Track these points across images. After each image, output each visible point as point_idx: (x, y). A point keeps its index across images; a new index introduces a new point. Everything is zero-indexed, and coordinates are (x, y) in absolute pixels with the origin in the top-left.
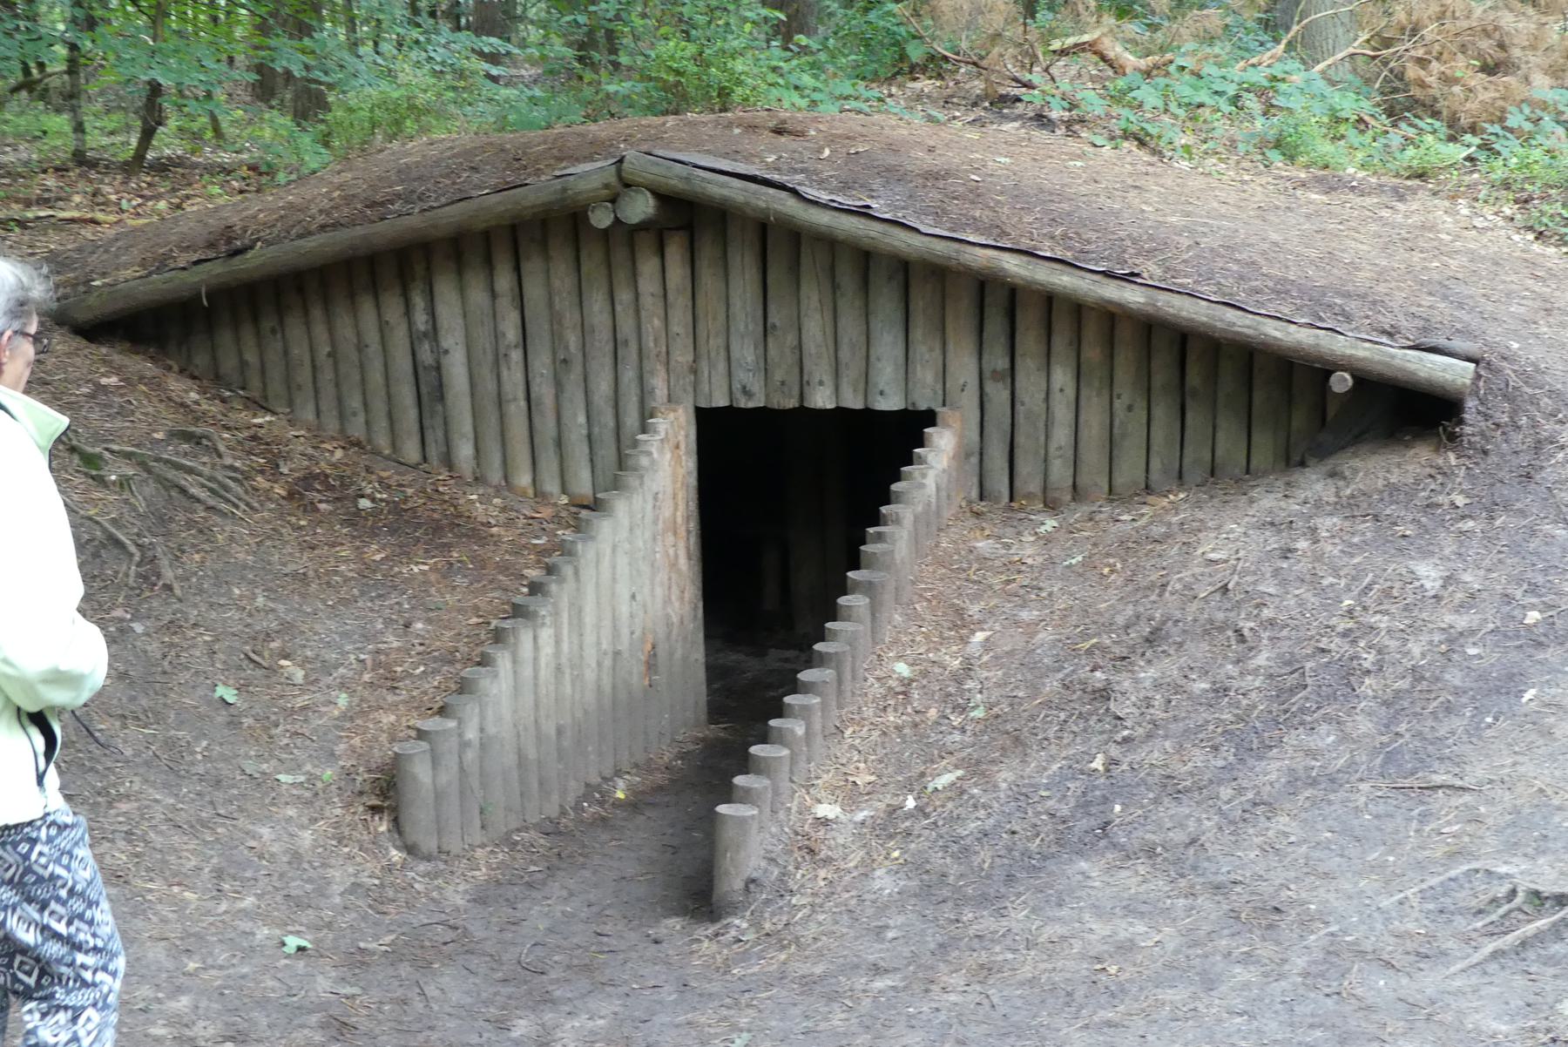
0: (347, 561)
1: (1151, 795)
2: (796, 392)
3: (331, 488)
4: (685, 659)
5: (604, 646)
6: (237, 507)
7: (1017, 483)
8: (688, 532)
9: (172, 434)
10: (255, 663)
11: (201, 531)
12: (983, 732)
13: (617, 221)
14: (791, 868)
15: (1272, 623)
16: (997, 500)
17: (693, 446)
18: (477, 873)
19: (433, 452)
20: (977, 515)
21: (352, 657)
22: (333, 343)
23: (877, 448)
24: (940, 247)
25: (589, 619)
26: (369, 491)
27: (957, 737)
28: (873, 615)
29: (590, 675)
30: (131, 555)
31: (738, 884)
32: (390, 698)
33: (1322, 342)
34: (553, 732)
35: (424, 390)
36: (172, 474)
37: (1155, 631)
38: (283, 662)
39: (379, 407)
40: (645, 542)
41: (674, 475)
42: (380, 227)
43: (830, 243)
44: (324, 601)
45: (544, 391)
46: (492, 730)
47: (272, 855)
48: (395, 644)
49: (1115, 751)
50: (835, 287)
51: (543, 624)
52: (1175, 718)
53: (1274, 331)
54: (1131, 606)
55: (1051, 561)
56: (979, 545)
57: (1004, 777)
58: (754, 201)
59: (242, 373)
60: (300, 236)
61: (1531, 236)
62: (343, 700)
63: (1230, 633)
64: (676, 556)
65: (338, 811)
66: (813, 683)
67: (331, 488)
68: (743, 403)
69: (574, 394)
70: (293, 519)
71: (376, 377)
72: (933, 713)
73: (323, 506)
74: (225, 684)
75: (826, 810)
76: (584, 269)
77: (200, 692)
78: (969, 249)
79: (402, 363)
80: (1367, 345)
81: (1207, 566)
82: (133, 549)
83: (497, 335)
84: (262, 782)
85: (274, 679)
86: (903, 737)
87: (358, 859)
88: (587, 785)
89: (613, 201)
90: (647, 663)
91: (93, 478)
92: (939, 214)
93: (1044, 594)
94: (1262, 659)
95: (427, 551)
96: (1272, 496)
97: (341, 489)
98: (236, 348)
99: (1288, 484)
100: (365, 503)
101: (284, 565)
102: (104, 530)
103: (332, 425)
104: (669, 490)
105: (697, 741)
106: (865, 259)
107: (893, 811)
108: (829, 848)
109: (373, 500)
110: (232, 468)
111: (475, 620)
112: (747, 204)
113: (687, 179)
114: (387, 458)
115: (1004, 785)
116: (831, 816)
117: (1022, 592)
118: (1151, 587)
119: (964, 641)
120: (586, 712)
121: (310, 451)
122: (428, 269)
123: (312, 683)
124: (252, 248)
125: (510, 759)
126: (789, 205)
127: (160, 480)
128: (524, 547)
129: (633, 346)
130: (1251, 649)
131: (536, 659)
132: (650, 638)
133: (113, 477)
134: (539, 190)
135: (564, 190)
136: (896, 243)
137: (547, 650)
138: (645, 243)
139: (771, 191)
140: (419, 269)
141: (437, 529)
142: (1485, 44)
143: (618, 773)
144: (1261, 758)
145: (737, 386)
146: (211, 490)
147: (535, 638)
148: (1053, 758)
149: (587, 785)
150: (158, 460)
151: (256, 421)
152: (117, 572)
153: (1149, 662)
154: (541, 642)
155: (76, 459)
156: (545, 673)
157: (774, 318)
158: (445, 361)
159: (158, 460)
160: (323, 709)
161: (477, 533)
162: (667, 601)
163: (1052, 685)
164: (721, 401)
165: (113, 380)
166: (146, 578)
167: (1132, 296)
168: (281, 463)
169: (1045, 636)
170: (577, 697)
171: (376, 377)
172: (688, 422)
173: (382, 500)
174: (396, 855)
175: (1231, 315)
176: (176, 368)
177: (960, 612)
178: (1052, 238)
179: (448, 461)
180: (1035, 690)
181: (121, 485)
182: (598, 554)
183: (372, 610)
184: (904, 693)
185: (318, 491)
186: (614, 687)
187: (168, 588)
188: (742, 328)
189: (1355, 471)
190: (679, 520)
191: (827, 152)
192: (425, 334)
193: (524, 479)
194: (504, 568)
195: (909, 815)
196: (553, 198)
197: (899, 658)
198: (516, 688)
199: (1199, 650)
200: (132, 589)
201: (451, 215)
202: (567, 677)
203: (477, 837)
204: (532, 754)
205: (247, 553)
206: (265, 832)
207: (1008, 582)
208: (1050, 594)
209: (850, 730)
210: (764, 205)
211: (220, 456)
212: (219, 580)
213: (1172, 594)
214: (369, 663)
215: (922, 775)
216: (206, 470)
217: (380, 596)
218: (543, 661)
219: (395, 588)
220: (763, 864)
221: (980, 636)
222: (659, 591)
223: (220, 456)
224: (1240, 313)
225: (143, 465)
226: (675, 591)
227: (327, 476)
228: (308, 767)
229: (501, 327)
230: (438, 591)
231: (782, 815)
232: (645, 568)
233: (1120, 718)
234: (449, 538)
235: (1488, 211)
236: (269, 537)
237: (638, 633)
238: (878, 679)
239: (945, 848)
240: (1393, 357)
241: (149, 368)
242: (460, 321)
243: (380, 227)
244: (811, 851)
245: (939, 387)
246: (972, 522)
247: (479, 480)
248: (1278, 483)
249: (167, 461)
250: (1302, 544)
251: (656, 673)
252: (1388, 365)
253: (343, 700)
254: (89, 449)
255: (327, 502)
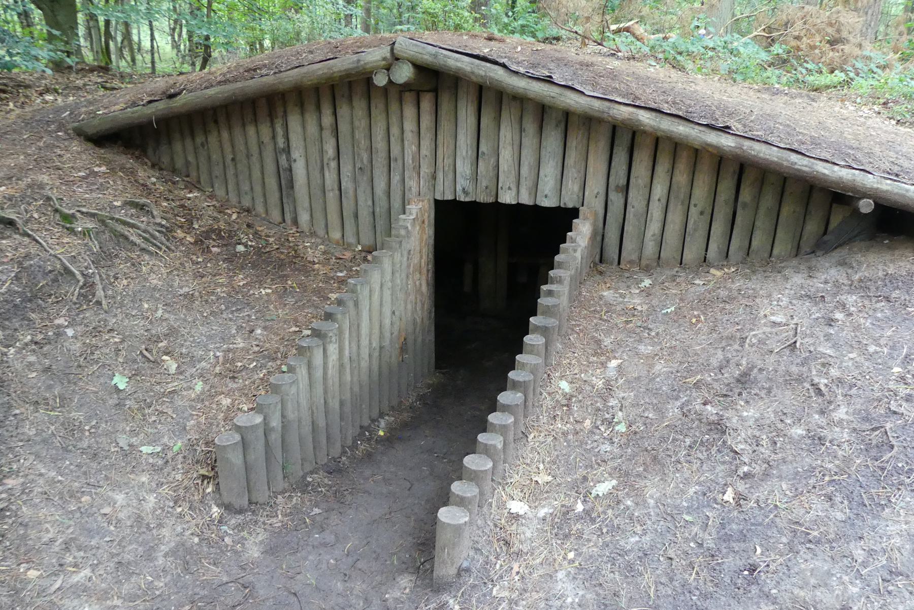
0: (222, 285)
1: (784, 540)
2: (494, 193)
3: (222, 238)
4: (423, 340)
5: (374, 345)
6: (160, 249)
7: (624, 254)
8: (428, 271)
9: (126, 203)
10: (144, 363)
11: (133, 265)
12: (627, 445)
13: (390, 82)
14: (492, 558)
15: (840, 381)
16: (612, 264)
17: (433, 221)
18: (274, 520)
19: (288, 217)
20: (601, 273)
21: (212, 353)
22: (234, 152)
23: (543, 229)
24: (597, 104)
25: (364, 330)
26: (244, 241)
27: (607, 447)
28: (546, 348)
29: (364, 364)
30: (79, 281)
31: (453, 571)
32: (232, 385)
33: (858, 179)
34: (337, 406)
35: (283, 182)
36: (120, 228)
37: (745, 374)
38: (165, 358)
39: (258, 189)
40: (402, 280)
41: (421, 239)
42: (251, 83)
43: (520, 100)
44: (201, 313)
45: (347, 184)
46: (291, 415)
47: (119, 521)
48: (241, 345)
49: (742, 487)
50: (521, 130)
51: (331, 342)
52: (784, 461)
53: (823, 169)
54: (720, 352)
55: (653, 309)
56: (605, 294)
57: (652, 491)
58: (476, 71)
59: (188, 167)
60: (206, 88)
61: (894, 122)
62: (199, 386)
63: (807, 385)
64: (421, 284)
65: (179, 477)
66: (508, 406)
67: (222, 238)
68: (462, 198)
69: (364, 188)
70: (194, 258)
71: (256, 174)
72: (588, 423)
73: (215, 250)
74: (120, 373)
75: (517, 507)
76: (373, 115)
77: (102, 380)
78: (617, 106)
79: (270, 167)
80: (889, 182)
81: (772, 327)
82: (80, 277)
83: (322, 151)
84: (130, 453)
85: (155, 371)
86: (568, 441)
87: (188, 518)
88: (361, 427)
89: (388, 70)
90: (402, 348)
91: (68, 229)
92: (594, 85)
93: (653, 334)
94: (841, 413)
95: (272, 280)
96: (800, 275)
97: (227, 238)
98: (181, 151)
99: (810, 268)
100: (240, 248)
101: (181, 288)
102: (63, 264)
103: (234, 199)
104: (418, 248)
105: (429, 386)
106: (543, 111)
107: (567, 511)
108: (521, 542)
109: (246, 246)
110: (160, 225)
111: (294, 329)
112: (473, 73)
113: (435, 56)
114: (264, 219)
115: (651, 502)
116: (521, 513)
117: (638, 330)
118: (731, 338)
119: (604, 365)
120: (361, 387)
121: (215, 214)
122: (285, 112)
123: (181, 373)
124: (179, 93)
125: (307, 429)
126: (498, 74)
127: (113, 231)
128: (332, 278)
129: (400, 162)
130: (830, 402)
131: (325, 364)
132: (403, 334)
133: (80, 229)
134: (344, 63)
135: (359, 61)
136: (568, 101)
137: (333, 356)
138: (409, 97)
139: (488, 65)
140: (280, 111)
141: (281, 265)
142: (830, 30)
143: (381, 415)
144: (876, 517)
145: (459, 188)
146: (144, 238)
147: (325, 351)
148: (687, 482)
149: (361, 427)
150: (112, 219)
151: (191, 195)
152: (67, 292)
153: (747, 402)
154: (329, 353)
155: (58, 217)
156: (332, 371)
157: (483, 148)
158: (294, 166)
159: (112, 219)
160: (185, 393)
161: (306, 268)
162: (414, 310)
163: (673, 411)
164: (449, 197)
165: (103, 169)
166: (85, 296)
167: (726, 142)
168: (195, 223)
169: (660, 367)
170: (355, 379)
171: (256, 174)
172: (430, 207)
173: (251, 246)
174: (215, 511)
175: (794, 157)
176: (149, 164)
177: (598, 342)
178: (667, 103)
179: (295, 222)
180: (660, 412)
181: (84, 234)
182: (370, 291)
183: (231, 320)
184: (567, 406)
185: (214, 240)
186: (380, 367)
187: (99, 303)
188: (464, 153)
189: (860, 263)
190: (423, 264)
191: (519, 49)
192: (283, 150)
193: (336, 235)
194: (318, 292)
195: (579, 518)
196: (351, 66)
197: (562, 377)
198: (311, 385)
199: (788, 398)
200: (75, 304)
201: (291, 77)
202: (348, 370)
203: (281, 484)
204: (322, 423)
205: (159, 279)
206: (120, 498)
207: (627, 322)
208: (657, 334)
209: (532, 435)
210: (483, 74)
211: (153, 217)
212: (136, 299)
213: (751, 346)
214: (221, 359)
215: (585, 479)
216: (143, 226)
217: (237, 310)
218: (330, 365)
219: (248, 304)
220: (472, 553)
221: (614, 363)
222: (409, 307)
223: (153, 217)
224: (800, 156)
225: (103, 222)
226: (419, 304)
227: (220, 231)
228: (165, 440)
229: (325, 148)
230: (275, 307)
231: (485, 509)
232: (401, 295)
233: (736, 452)
234: (288, 271)
235: (865, 109)
236: (177, 269)
237: (396, 333)
238: (549, 394)
239: (613, 561)
240: (907, 191)
241: (130, 162)
242: (302, 143)
243: (251, 83)
244: (507, 543)
245: (581, 194)
246: (598, 277)
247: (313, 234)
248: (802, 267)
249: (117, 220)
250: (839, 316)
251: (407, 353)
252: (904, 196)
253: (199, 386)
254: (67, 211)
255: (218, 246)
